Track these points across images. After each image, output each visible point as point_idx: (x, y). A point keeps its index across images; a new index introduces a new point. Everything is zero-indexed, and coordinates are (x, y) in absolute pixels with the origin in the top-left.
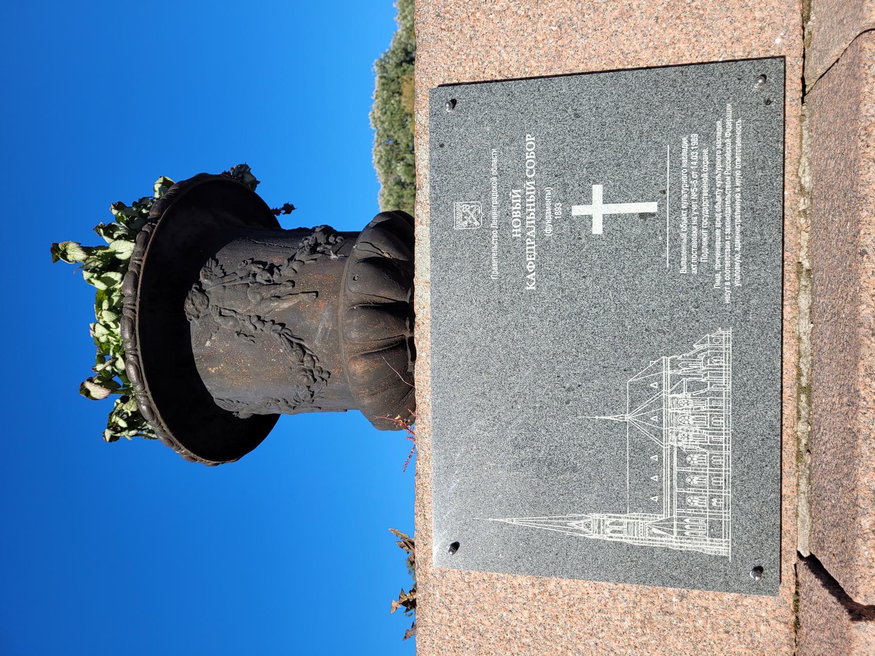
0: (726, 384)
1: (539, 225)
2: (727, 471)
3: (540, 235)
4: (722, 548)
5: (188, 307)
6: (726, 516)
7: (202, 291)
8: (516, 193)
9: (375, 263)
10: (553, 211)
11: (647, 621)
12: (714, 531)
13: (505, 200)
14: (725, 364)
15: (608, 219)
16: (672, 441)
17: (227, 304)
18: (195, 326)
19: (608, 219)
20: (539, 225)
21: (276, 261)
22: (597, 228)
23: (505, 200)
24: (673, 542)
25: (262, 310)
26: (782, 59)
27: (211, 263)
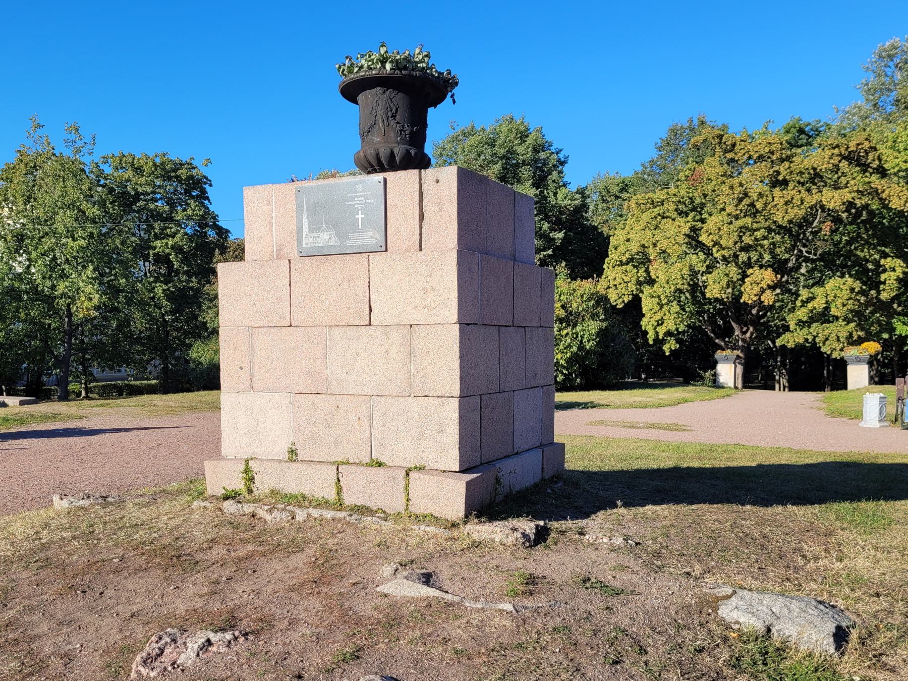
0: (331, 244)
1: (358, 204)
2: (317, 245)
3: (355, 204)
4: (304, 245)
5: (378, 88)
6: (309, 246)
7: (384, 92)
8: (363, 198)
9: (392, 155)
10: (360, 207)
11: (292, 233)
12: (307, 244)
13: (362, 196)
14: (334, 244)
15: (358, 218)
16: (320, 234)
17: (381, 102)
18: (373, 91)
19: (358, 218)
20: (358, 204)
21: (398, 117)
22: (357, 217)
23: (362, 196)
24: (304, 236)
25: (379, 116)
26: (383, 249)
27: (396, 92)
